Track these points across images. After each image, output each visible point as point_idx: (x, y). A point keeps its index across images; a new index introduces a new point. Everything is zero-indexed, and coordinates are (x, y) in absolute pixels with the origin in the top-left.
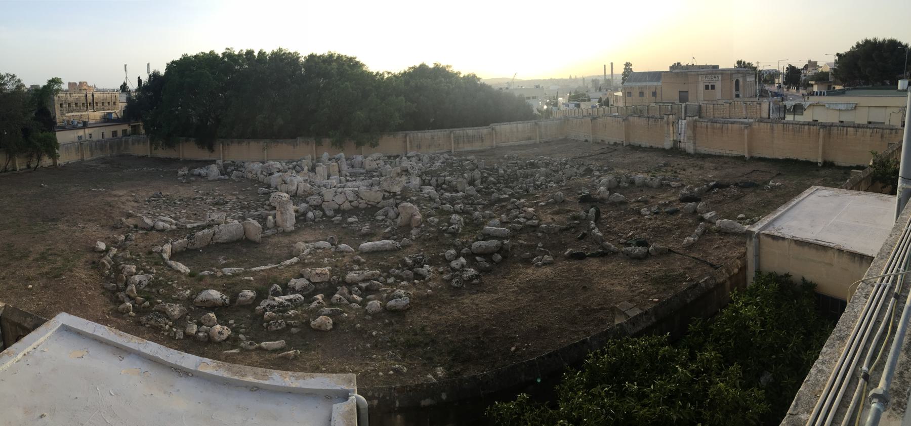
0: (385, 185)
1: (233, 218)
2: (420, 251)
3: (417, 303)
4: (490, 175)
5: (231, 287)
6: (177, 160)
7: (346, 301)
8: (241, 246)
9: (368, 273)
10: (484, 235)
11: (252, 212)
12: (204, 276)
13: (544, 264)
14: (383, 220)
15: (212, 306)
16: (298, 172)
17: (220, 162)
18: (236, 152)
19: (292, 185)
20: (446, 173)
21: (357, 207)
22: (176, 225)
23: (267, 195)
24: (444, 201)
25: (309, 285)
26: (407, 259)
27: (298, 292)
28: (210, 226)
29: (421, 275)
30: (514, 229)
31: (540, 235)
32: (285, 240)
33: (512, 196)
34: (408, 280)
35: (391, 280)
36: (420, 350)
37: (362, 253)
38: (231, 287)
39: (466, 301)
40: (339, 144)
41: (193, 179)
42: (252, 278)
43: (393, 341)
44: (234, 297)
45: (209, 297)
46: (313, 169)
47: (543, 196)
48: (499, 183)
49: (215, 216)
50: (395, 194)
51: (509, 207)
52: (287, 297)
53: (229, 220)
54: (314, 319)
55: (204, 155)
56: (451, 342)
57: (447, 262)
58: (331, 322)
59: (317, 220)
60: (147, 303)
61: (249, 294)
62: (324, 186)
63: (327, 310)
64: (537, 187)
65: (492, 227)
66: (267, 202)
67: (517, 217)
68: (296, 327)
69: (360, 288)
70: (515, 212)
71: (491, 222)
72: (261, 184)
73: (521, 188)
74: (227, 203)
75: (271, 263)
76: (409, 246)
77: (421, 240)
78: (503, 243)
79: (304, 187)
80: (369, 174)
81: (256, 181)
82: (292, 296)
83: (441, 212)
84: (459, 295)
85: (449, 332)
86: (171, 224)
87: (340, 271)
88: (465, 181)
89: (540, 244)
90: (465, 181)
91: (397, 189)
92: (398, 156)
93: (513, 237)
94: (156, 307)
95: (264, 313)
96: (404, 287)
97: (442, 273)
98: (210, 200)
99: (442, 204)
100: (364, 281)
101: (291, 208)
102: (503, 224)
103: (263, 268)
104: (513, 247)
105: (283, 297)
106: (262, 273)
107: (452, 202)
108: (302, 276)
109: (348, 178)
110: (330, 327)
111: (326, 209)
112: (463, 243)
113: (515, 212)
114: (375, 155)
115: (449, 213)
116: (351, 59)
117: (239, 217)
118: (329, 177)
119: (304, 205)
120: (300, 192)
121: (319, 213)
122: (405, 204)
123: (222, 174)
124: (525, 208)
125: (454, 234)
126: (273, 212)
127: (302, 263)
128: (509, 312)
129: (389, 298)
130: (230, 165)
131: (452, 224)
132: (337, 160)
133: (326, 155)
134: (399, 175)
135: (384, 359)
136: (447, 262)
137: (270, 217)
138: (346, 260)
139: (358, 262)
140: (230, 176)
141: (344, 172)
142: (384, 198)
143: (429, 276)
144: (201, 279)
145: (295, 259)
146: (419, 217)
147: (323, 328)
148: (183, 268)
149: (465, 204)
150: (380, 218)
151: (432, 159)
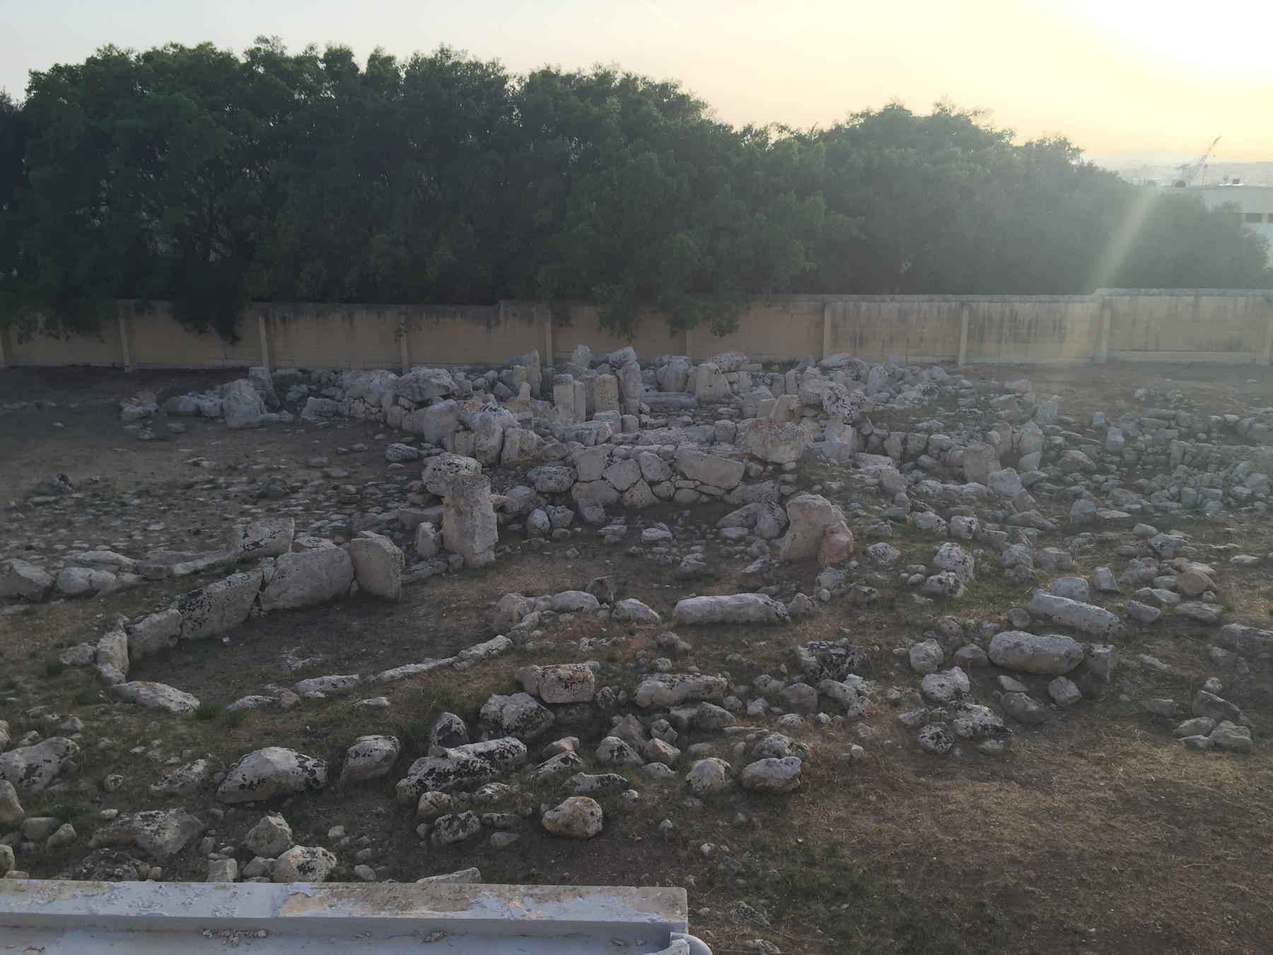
0: (754, 442)
1: (318, 533)
2: (841, 634)
3: (822, 777)
4: (1075, 443)
5: (325, 732)
6: (115, 372)
7: (635, 757)
8: (348, 613)
9: (695, 680)
10: (1034, 616)
11: (373, 513)
12: (245, 710)
13: (1217, 747)
14: (741, 539)
15: (275, 795)
16: (501, 399)
17: (261, 371)
18: (312, 341)
19: (489, 434)
20: (935, 423)
21: (670, 499)
22: (136, 570)
23: (415, 463)
24: (919, 500)
25: (538, 712)
26: (804, 653)
27: (509, 732)
28: (246, 563)
29: (836, 701)
30: (1132, 618)
31: (1218, 652)
32: (470, 591)
33: (1143, 515)
34: (802, 709)
35: (757, 707)
36: (819, 906)
37: (682, 626)
38: (325, 732)
39: (956, 795)
40: (620, 324)
41: (177, 426)
42: (384, 701)
43: (750, 874)
44: (337, 757)
45: (265, 771)
46: (545, 392)
47: (1252, 534)
48: (1104, 471)
49: (263, 531)
50: (779, 468)
51: (1128, 547)
52: (480, 747)
53: (304, 539)
54: (553, 805)
55: (206, 351)
56: (906, 901)
57: (913, 675)
58: (599, 811)
59: (557, 533)
60: (67, 830)
61: (380, 745)
62: (579, 438)
63: (588, 779)
64: (1234, 503)
65: (1062, 596)
66: (416, 484)
67: (1149, 582)
68: (505, 829)
69: (675, 722)
70: (1143, 567)
71: (1063, 581)
72: (394, 431)
73: (1177, 498)
74: (295, 490)
75: (434, 656)
76: (809, 616)
77: (849, 604)
78: (1089, 652)
79: (522, 439)
80: (706, 409)
81: (379, 426)
82: (493, 744)
83: (908, 532)
84: (939, 776)
85: (902, 872)
86: (119, 569)
87: (621, 671)
88: (990, 451)
89: (1213, 683)
90: (990, 451)
91: (787, 455)
92: (792, 364)
93: (1127, 640)
94: (100, 834)
95: (419, 794)
96: (789, 729)
97: (896, 704)
98: (239, 485)
99: (914, 508)
100: (686, 702)
101: (487, 498)
102: (1098, 594)
103: (411, 668)
104: (1121, 670)
105: (470, 747)
106: (409, 684)
107: (945, 507)
108: (518, 687)
109: (645, 419)
110: (594, 827)
111: (581, 501)
112: (965, 628)
113: (1143, 567)
114: (728, 358)
115: (932, 537)
116: (664, 88)
117: (336, 531)
118: (590, 415)
119: (522, 491)
120: (511, 453)
121: (563, 514)
122: (806, 497)
123: (272, 408)
124: (1179, 561)
125: (942, 599)
126: (433, 512)
127: (517, 651)
128: (1080, 857)
129: (752, 755)
130: (295, 380)
131: (938, 570)
132: (615, 367)
133: (582, 352)
134: (794, 416)
135: (728, 921)
136: (913, 675)
137: (426, 526)
138: (639, 643)
139: (669, 650)
140: (297, 413)
141: (634, 403)
142: (747, 478)
143: (857, 707)
144: (235, 721)
145: (500, 641)
146: (844, 537)
147: (577, 828)
148: (173, 697)
149: (983, 518)
150: (733, 532)
151: (896, 380)
